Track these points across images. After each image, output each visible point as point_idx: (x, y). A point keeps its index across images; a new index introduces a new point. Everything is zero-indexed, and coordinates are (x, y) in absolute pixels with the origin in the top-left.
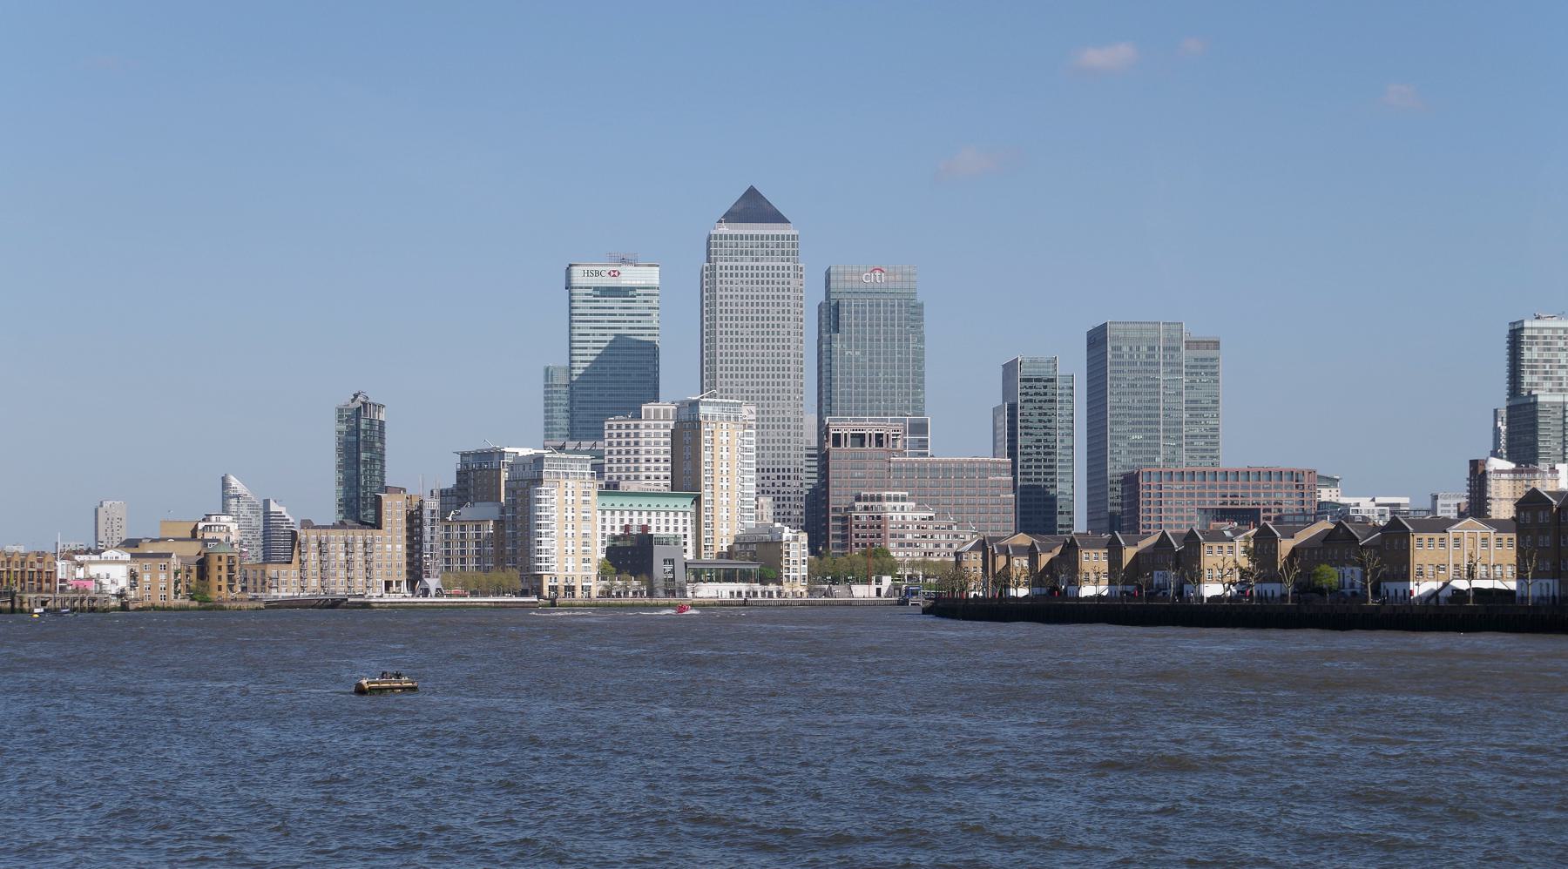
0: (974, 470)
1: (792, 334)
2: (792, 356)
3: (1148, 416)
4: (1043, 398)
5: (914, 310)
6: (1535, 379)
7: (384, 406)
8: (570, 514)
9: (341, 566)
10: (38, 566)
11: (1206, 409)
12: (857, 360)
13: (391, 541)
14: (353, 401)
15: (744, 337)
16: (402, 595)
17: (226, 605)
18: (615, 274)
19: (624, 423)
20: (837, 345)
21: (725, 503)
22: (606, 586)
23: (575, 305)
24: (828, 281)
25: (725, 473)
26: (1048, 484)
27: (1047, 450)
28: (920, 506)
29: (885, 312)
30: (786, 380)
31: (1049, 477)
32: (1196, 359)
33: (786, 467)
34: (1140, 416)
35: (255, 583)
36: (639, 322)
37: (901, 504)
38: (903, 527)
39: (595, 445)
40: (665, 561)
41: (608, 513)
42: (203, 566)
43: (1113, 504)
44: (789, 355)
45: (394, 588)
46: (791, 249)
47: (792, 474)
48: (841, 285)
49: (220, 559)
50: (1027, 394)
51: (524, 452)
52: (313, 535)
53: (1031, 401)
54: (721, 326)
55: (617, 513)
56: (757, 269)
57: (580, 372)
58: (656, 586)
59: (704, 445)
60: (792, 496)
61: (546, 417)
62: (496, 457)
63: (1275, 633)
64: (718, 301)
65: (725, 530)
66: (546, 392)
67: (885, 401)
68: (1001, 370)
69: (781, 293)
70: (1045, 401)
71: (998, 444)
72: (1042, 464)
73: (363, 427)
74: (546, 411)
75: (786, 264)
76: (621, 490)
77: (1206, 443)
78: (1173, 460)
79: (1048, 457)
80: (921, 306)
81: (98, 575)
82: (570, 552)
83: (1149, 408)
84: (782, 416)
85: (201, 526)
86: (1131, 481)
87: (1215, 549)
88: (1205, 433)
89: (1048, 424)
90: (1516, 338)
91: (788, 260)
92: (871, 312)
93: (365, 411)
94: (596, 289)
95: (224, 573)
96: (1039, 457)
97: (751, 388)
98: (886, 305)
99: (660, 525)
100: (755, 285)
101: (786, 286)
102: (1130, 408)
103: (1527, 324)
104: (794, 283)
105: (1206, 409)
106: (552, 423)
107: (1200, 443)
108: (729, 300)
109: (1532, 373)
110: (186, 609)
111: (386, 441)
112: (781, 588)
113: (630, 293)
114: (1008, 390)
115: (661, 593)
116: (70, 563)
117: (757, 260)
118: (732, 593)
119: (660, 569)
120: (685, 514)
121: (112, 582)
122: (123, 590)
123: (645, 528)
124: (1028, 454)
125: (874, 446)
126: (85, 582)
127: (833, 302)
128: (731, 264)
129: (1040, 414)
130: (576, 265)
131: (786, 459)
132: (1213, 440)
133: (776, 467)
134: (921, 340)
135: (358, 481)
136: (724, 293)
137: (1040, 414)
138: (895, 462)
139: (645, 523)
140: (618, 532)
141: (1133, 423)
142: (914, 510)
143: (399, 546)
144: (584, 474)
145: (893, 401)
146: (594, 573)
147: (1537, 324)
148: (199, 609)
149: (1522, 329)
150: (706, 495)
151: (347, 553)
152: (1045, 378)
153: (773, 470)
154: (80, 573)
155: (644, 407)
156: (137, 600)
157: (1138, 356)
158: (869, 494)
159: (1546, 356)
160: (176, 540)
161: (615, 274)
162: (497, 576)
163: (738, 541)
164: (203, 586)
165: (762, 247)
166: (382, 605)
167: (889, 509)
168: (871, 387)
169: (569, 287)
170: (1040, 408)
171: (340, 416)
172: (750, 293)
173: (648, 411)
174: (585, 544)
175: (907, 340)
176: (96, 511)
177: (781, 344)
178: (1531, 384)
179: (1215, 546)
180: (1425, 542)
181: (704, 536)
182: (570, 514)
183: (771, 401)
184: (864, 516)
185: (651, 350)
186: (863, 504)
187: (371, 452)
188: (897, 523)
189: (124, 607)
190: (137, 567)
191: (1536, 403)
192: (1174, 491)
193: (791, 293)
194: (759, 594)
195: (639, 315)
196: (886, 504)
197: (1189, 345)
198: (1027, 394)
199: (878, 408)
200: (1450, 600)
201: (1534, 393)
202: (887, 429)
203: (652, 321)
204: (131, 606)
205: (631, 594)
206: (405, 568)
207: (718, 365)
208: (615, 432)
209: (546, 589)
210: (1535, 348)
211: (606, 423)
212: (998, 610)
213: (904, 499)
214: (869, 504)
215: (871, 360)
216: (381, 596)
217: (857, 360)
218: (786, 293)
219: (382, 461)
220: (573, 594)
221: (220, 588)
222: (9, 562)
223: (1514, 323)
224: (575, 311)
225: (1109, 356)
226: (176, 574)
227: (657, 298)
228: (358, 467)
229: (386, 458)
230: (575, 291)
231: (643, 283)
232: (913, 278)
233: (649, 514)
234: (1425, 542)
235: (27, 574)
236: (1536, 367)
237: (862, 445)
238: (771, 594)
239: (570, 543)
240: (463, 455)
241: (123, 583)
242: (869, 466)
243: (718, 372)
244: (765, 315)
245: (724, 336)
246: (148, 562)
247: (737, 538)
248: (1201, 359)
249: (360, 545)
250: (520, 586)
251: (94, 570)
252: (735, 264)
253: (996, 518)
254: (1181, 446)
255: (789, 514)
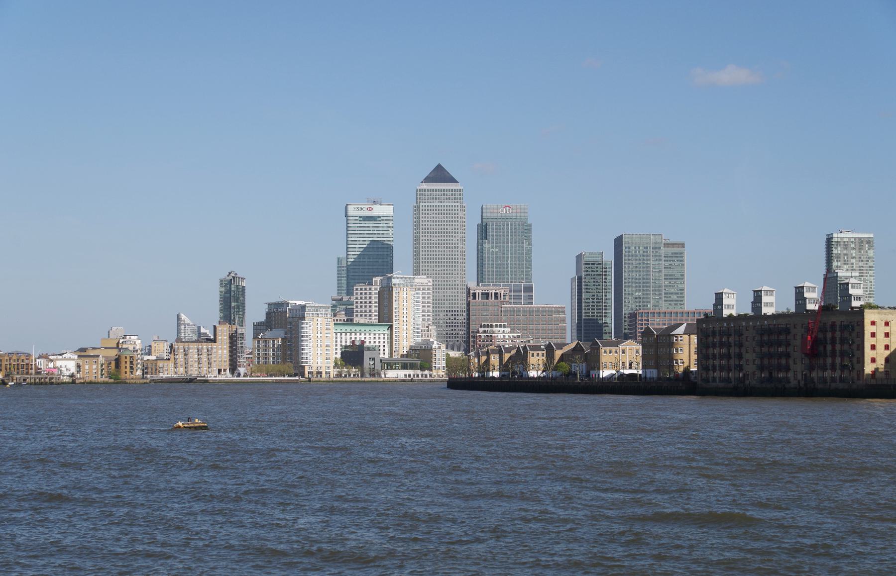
0: (545, 311)
1: (459, 240)
2: (459, 251)
3: (644, 283)
4: (596, 273)
5: (526, 228)
6: (839, 264)
7: (244, 279)
8: (319, 335)
9: (195, 361)
10: (26, 361)
11: (678, 279)
12: (496, 254)
13: (221, 349)
14: (228, 276)
15: (435, 242)
16: (227, 376)
17: (128, 381)
18: (370, 209)
19: (364, 287)
20: (486, 246)
21: (405, 329)
22: (338, 372)
23: (349, 225)
24: (482, 213)
25: (405, 313)
26: (599, 318)
27: (598, 300)
28: (512, 331)
29: (511, 229)
30: (456, 264)
31: (599, 315)
32: (672, 253)
33: (456, 309)
34: (640, 283)
35: (152, 370)
36: (383, 234)
37: (503, 329)
38: (504, 341)
39: (350, 298)
40: (370, 359)
41: (344, 334)
42: (118, 361)
43: (625, 329)
44: (458, 251)
45: (222, 372)
46: (459, 196)
47: (459, 313)
48: (488, 215)
49: (126, 358)
50: (587, 271)
51: (298, 303)
52: (181, 346)
53: (589, 275)
54: (422, 236)
55: (348, 334)
56: (452, 207)
57: (352, 260)
58: (365, 371)
59: (394, 299)
60: (459, 325)
61: (338, 284)
62: (285, 306)
63: (592, 397)
64: (421, 223)
65: (405, 343)
66: (338, 271)
67: (511, 275)
68: (575, 258)
69: (454, 219)
70: (597, 275)
71: (573, 297)
72: (595, 307)
73: (233, 289)
74: (338, 280)
75: (456, 204)
76: (355, 322)
77: (678, 297)
78: (658, 306)
79: (598, 304)
80: (530, 225)
81: (61, 366)
82: (319, 354)
83: (644, 279)
84: (454, 283)
85: (121, 341)
86: (633, 316)
87: (535, 354)
88: (677, 292)
89: (598, 287)
90: (829, 241)
91: (457, 202)
92: (504, 229)
93: (234, 281)
94: (360, 217)
95: (128, 365)
96: (594, 304)
97: (438, 269)
98: (511, 225)
99: (370, 341)
100: (440, 215)
101: (456, 216)
102: (635, 279)
103: (835, 235)
104: (461, 214)
105: (678, 279)
106: (341, 287)
107: (674, 297)
108: (427, 223)
109: (837, 261)
110: (107, 383)
111: (246, 297)
112: (431, 372)
113: (378, 219)
114: (578, 270)
115: (368, 375)
116: (45, 360)
117: (441, 202)
118: (406, 375)
119: (367, 363)
120: (384, 335)
121: (67, 370)
122: (73, 374)
123: (363, 342)
124: (588, 303)
125: (480, 299)
126: (53, 370)
127: (484, 224)
128: (428, 204)
129: (594, 282)
130: (350, 205)
131: (456, 305)
132: (681, 295)
133: (451, 309)
134: (530, 243)
135: (230, 317)
136: (424, 219)
137: (594, 282)
138: (504, 307)
139: (363, 339)
140: (348, 344)
141: (636, 287)
142: (511, 332)
143: (225, 351)
144: (327, 314)
145: (515, 275)
146: (332, 365)
147: (840, 235)
148: (114, 383)
149: (833, 238)
150: (395, 325)
151: (198, 355)
152: (597, 263)
153: (450, 311)
154: (51, 365)
155: (374, 279)
156: (80, 378)
157: (639, 252)
158: (486, 324)
159: (845, 252)
160: (105, 348)
161: (370, 209)
162: (281, 367)
163: (411, 348)
164: (117, 371)
165: (444, 195)
166: (214, 383)
167: (497, 332)
168: (504, 268)
169: (346, 216)
170: (594, 278)
171: (221, 284)
172: (437, 219)
173: (376, 281)
174: (327, 350)
175: (523, 243)
176: (109, 332)
177: (454, 246)
178: (837, 266)
179: (535, 353)
180: (608, 351)
181: (394, 346)
182: (319, 335)
183: (448, 275)
184: (483, 336)
185: (389, 249)
186: (483, 329)
187: (237, 302)
188: (500, 339)
189: (73, 382)
190: (81, 362)
191: (837, 276)
192: (655, 322)
193: (459, 219)
194: (420, 376)
195: (383, 230)
196: (495, 329)
197: (667, 245)
198: (587, 271)
199: (508, 279)
200: (618, 378)
201: (836, 271)
202: (501, 290)
203: (389, 234)
204: (77, 382)
205: (352, 376)
206: (228, 363)
207: (421, 257)
208: (359, 292)
209: (306, 373)
210: (839, 248)
211: (355, 288)
212: (485, 385)
213: (504, 327)
214: (486, 329)
215: (504, 254)
216: (216, 377)
217: (496, 254)
218: (456, 219)
219: (244, 307)
220: (321, 376)
221: (126, 373)
222: (10, 359)
223: (829, 235)
224: (349, 229)
225: (624, 252)
226: (102, 365)
227: (392, 222)
228: (230, 310)
229: (246, 305)
230: (349, 218)
231: (385, 214)
232: (526, 211)
233: (365, 334)
234: (608, 351)
235: (20, 365)
236: (840, 258)
237: (487, 299)
238: (426, 376)
239: (319, 349)
240: (269, 304)
241: (73, 370)
242: (491, 309)
243: (421, 260)
244: (446, 231)
245: (424, 242)
246: (87, 360)
247: (411, 347)
248: (675, 253)
249: (205, 350)
250: (293, 372)
251: (58, 364)
252: (429, 204)
253: (557, 336)
254: (661, 298)
255: (458, 334)
